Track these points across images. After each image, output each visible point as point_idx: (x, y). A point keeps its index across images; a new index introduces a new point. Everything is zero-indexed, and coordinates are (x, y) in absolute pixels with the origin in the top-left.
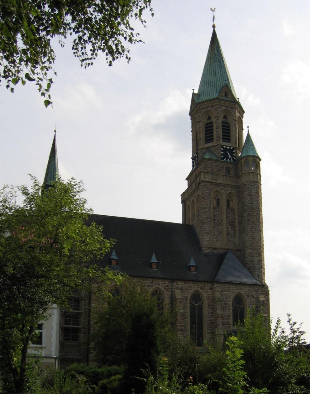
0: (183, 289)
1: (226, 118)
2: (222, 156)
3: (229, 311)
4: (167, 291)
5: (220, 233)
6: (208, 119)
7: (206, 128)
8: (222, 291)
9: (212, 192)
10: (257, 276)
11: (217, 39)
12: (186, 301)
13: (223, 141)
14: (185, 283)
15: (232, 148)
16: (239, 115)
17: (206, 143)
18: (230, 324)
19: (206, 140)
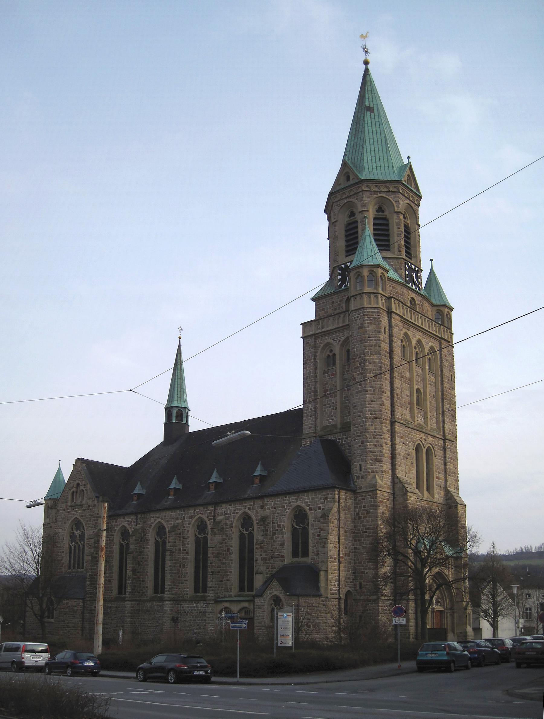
0: (228, 514)
3: (283, 537)
4: (210, 519)
5: (333, 409)
6: (350, 217)
7: (346, 231)
8: (275, 508)
9: (319, 350)
10: (358, 467)
11: (371, 81)
12: (231, 530)
14: (231, 505)
16: (408, 202)
17: (346, 256)
18: (283, 556)
19: (347, 251)
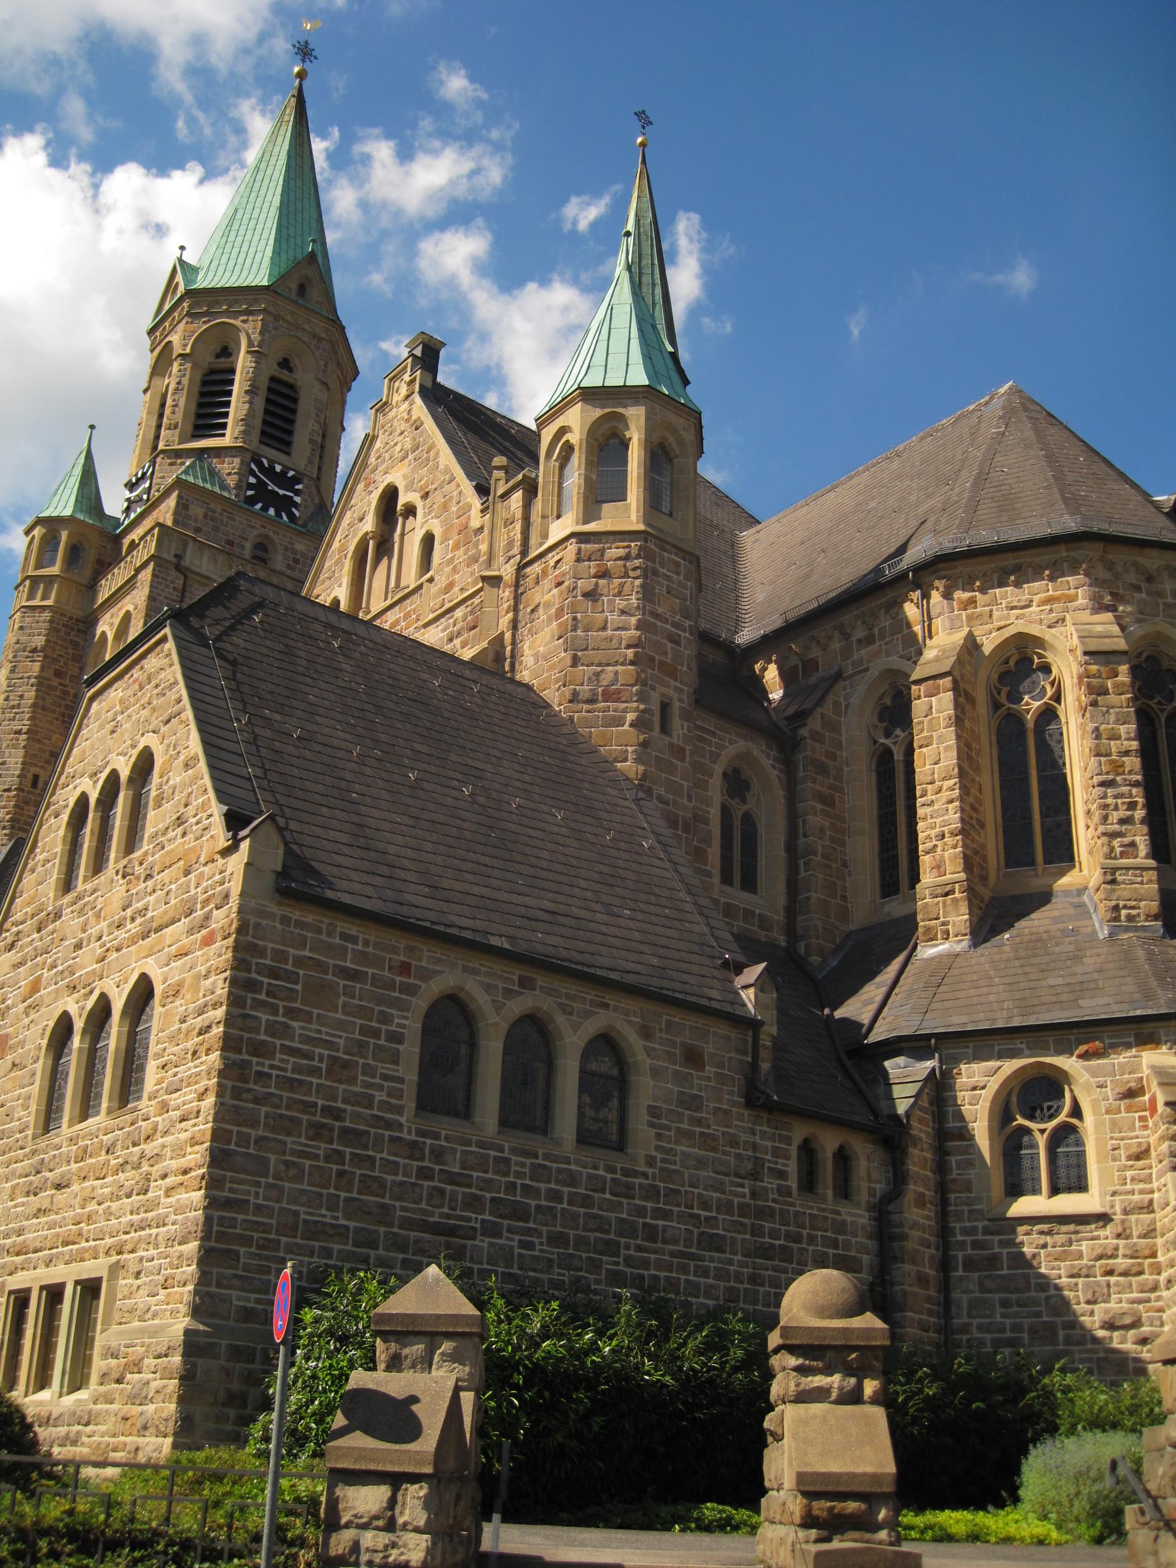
1: (290, 370)
2: (250, 493)
6: (218, 356)
13: (261, 442)
15: (291, 473)
19: (197, 427)
